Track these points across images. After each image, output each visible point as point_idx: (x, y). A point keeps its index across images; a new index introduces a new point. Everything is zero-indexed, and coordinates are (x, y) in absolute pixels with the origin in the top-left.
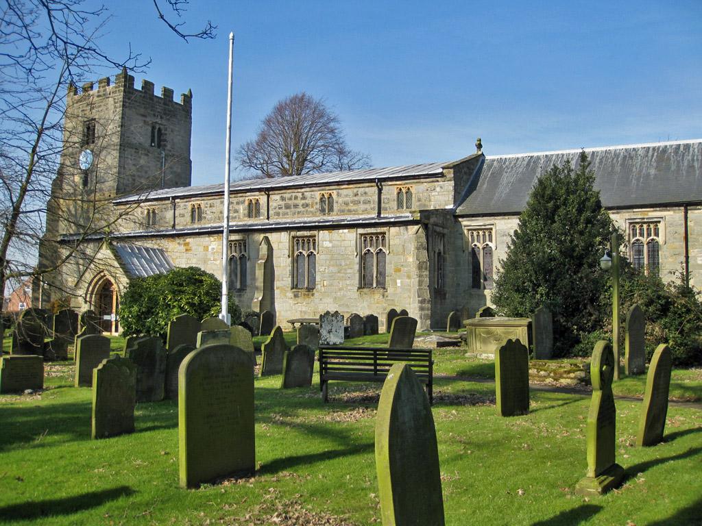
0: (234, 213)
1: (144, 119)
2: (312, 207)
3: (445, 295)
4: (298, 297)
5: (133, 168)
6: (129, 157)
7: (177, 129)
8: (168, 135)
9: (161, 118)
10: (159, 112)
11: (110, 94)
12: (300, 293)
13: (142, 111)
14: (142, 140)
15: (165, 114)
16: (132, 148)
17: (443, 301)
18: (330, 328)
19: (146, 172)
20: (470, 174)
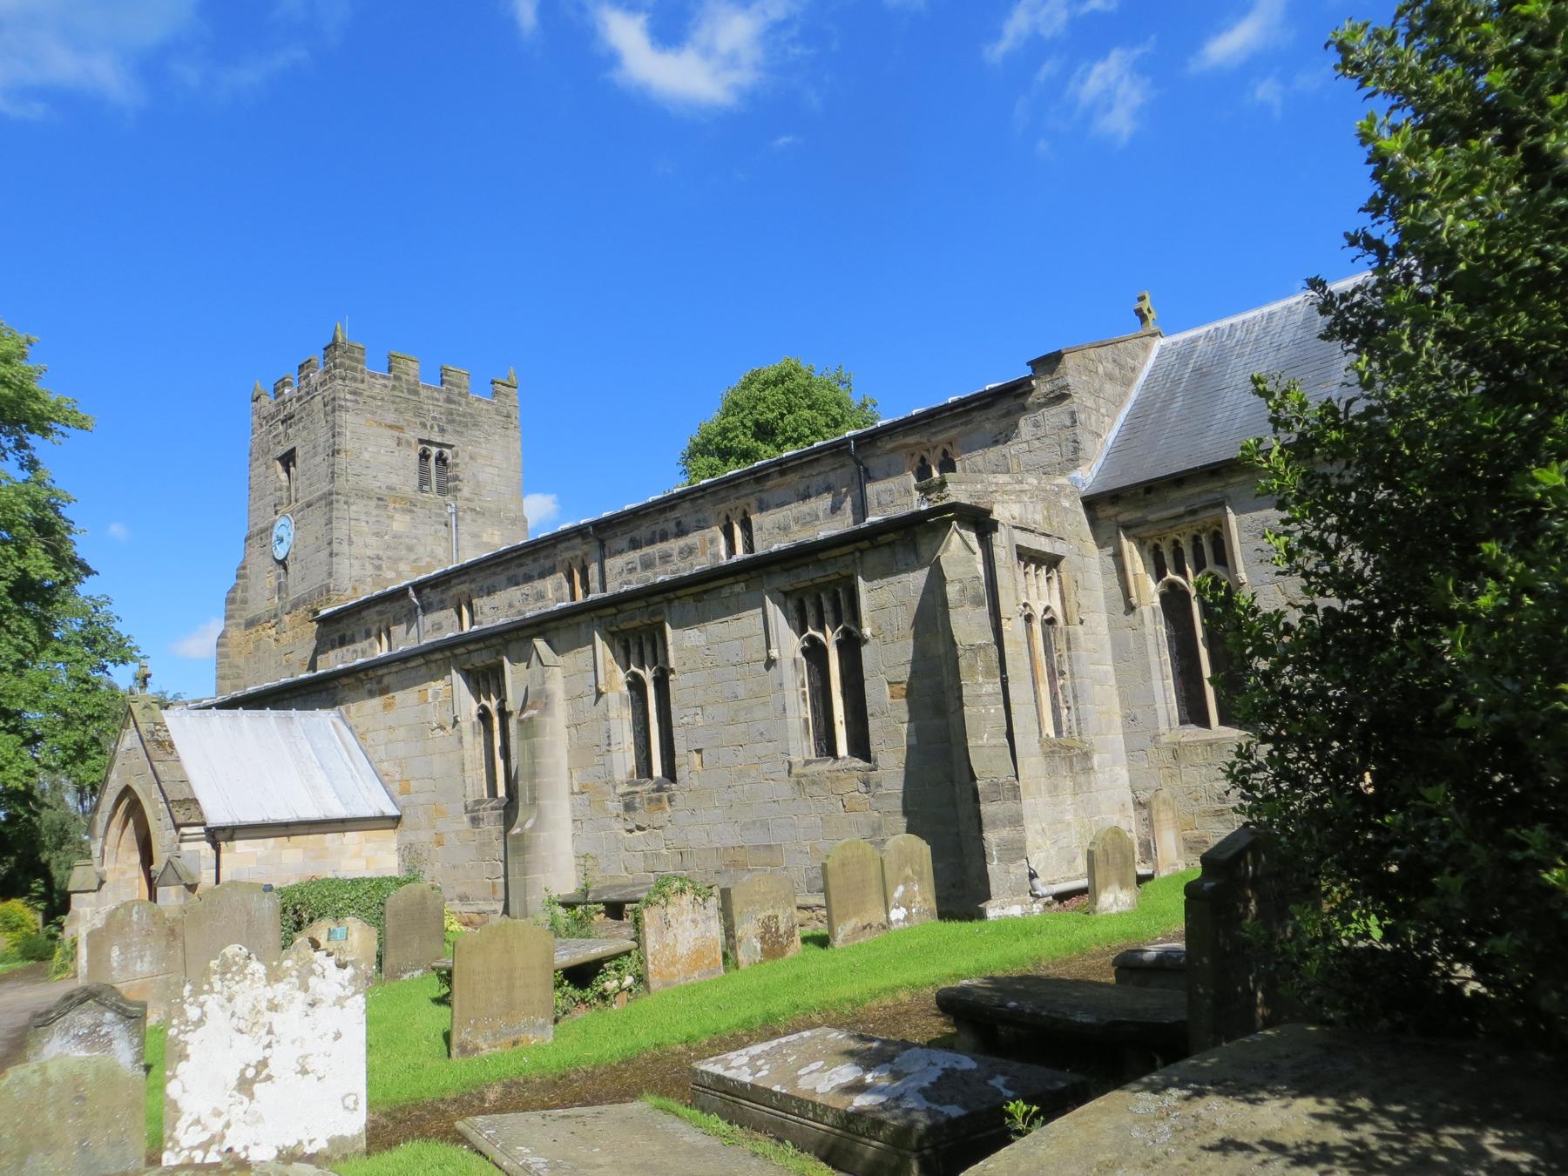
0: (537, 600)
1: (396, 434)
2: (704, 553)
3: (1086, 756)
4: (634, 809)
5: (373, 540)
6: (363, 517)
7: (484, 452)
8: (462, 466)
9: (442, 430)
10: (434, 418)
11: (316, 390)
12: (638, 800)
13: (391, 418)
14: (394, 480)
15: (449, 422)
16: (370, 498)
17: (1082, 779)
18: (256, 1055)
19: (410, 549)
20: (1128, 383)
